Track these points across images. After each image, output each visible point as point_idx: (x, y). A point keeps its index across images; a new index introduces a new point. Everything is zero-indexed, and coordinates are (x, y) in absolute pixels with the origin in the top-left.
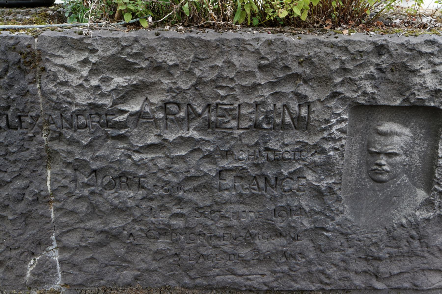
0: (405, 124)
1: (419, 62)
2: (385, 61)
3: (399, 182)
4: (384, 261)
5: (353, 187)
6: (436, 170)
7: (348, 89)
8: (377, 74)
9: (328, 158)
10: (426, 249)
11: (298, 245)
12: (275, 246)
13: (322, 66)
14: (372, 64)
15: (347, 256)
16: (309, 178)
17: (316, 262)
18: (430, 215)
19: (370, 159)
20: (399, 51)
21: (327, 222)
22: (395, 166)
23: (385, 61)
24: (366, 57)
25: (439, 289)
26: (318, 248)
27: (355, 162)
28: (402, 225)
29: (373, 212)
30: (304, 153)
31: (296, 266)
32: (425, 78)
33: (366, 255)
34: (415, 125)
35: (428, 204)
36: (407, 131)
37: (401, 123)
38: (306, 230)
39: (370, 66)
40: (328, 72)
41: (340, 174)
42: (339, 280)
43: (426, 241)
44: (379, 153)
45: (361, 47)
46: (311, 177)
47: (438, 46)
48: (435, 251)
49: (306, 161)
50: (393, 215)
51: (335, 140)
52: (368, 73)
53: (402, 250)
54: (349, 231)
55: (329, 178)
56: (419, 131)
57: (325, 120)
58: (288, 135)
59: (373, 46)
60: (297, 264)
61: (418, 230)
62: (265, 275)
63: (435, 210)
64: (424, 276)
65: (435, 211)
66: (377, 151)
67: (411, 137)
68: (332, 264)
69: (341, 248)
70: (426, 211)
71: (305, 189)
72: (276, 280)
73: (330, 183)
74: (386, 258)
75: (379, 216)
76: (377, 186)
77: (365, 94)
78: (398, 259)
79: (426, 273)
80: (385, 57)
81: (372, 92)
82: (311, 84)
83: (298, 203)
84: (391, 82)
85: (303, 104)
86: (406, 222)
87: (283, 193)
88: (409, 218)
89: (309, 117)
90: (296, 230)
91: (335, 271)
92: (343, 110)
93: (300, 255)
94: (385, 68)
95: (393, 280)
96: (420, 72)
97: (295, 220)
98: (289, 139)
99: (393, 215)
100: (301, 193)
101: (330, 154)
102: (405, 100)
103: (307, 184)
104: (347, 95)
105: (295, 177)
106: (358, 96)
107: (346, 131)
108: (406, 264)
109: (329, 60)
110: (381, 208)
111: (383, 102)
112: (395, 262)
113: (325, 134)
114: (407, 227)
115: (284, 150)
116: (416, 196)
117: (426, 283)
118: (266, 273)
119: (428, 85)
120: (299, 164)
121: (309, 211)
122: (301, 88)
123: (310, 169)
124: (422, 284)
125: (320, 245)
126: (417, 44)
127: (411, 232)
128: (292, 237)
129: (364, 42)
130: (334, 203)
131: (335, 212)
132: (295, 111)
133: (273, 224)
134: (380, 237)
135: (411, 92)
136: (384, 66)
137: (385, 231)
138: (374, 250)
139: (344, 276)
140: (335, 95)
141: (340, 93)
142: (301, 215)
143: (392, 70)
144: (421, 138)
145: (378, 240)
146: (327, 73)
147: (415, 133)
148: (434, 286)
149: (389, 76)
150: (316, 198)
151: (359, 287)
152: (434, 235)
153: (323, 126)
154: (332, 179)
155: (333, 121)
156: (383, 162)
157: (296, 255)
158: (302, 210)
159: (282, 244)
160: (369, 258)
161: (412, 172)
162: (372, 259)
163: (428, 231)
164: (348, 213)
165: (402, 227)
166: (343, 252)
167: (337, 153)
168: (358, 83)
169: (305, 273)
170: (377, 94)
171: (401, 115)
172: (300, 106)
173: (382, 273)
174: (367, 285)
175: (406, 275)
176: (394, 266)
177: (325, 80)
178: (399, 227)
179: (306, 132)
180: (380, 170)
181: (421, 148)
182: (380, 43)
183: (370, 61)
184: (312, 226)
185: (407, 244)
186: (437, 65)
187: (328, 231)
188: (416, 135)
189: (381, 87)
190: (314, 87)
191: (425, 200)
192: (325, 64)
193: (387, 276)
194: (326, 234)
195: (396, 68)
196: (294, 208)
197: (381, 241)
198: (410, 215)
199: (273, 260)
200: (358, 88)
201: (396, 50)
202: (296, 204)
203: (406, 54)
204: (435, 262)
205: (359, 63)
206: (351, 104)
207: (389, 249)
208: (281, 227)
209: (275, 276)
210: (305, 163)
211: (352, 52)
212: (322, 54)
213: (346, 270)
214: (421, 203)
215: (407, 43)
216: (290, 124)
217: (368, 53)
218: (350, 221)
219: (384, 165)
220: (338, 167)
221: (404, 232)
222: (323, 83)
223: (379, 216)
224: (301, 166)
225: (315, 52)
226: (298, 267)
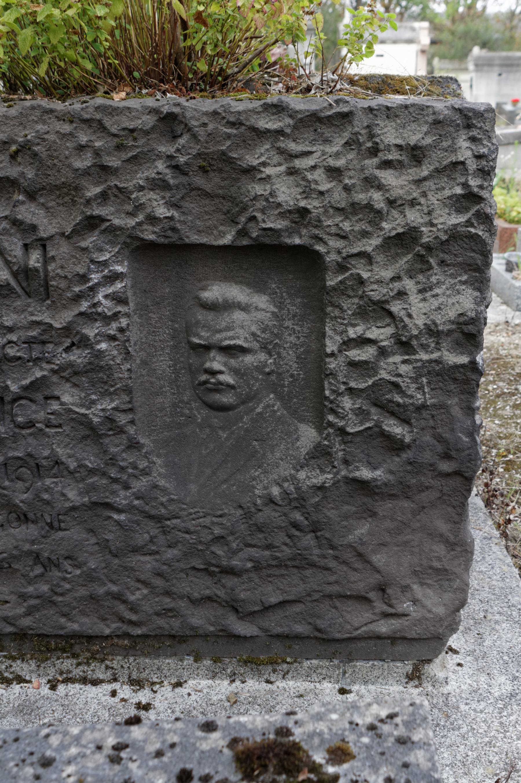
0: (259, 287)
1: (257, 151)
2: (183, 149)
3: (259, 410)
4: (245, 577)
5: (168, 420)
6: (326, 383)
7: (118, 211)
8: (173, 177)
9: (97, 356)
10: (331, 552)
11: (62, 539)
12: (17, 541)
13: (55, 161)
14: (159, 156)
15: (164, 564)
16: (66, 398)
17: (102, 577)
18: (326, 478)
19: (194, 361)
20: (211, 127)
21: (114, 493)
22: (244, 374)
23: (183, 149)
24: (144, 140)
25: (370, 638)
26: (104, 546)
27: (165, 366)
28: (271, 501)
29: (214, 473)
30: (50, 347)
31: (62, 583)
32: (273, 184)
33: (205, 564)
34: (279, 288)
35: (320, 454)
36: (261, 301)
37: (248, 285)
38: (74, 509)
39: (155, 160)
40: (69, 175)
41: (128, 390)
42: (158, 614)
43: (327, 535)
44: (207, 348)
45: (131, 120)
46: (69, 396)
47: (291, 116)
48: (348, 555)
49: (54, 363)
50: (254, 479)
51: (107, 319)
52: (153, 175)
53: (278, 554)
54: (163, 511)
55: (108, 399)
56: (288, 301)
57: (78, 275)
58: (12, 308)
59: (156, 118)
60: (64, 579)
61: (304, 510)
62: (7, 602)
63: (334, 467)
64: (334, 610)
65: (335, 470)
66: (202, 342)
67: (273, 313)
68: (138, 581)
69: (153, 548)
70: (318, 471)
71: (61, 422)
72: (29, 613)
73: (108, 410)
74: (247, 571)
75: (225, 481)
76: (215, 417)
77: (152, 219)
78: (276, 573)
79: (338, 604)
80: (182, 141)
81: (167, 215)
82: (42, 201)
83: (49, 452)
84: (207, 195)
85: (31, 244)
86: (280, 493)
87: (17, 430)
88: (286, 485)
89: (46, 271)
90: (53, 507)
91: (145, 597)
92: (113, 254)
93: (70, 562)
94: (186, 163)
95: (273, 618)
96: (262, 172)
97: (49, 487)
98: (15, 316)
99: (254, 479)
100: (53, 430)
101: (98, 347)
102: (243, 233)
103: (63, 412)
104: (117, 222)
105: (39, 397)
106: (139, 224)
107: (127, 298)
108: (294, 585)
109: (68, 148)
110: (229, 465)
111: (196, 237)
112: (269, 579)
113: (84, 306)
114: (280, 503)
115: (5, 340)
116: (297, 439)
117: (340, 625)
118: (7, 598)
119: (281, 198)
120: (42, 369)
121: (75, 469)
122: (22, 208)
123: (68, 380)
124: (330, 626)
125: (108, 541)
126: (245, 112)
127: (292, 516)
128: (47, 524)
129: (138, 111)
130: (124, 451)
131: (130, 471)
132: (15, 257)
133: (6, 496)
134: (229, 524)
135: (247, 214)
136: (182, 159)
137: (240, 512)
138: (220, 552)
139: (165, 607)
140: (92, 223)
141: (102, 220)
142: (63, 477)
143: (202, 168)
144: (294, 316)
145: (226, 532)
146: (65, 176)
147: (280, 306)
148: (359, 632)
149: (199, 181)
150: (88, 442)
151: (201, 632)
152: (345, 523)
153: (77, 289)
154: (112, 401)
155: (95, 278)
156: (216, 366)
157: (61, 561)
158: (62, 467)
159: (29, 537)
160: (213, 569)
161: (286, 389)
162: (221, 572)
163: (328, 514)
164: (160, 474)
165: (272, 505)
166: (157, 557)
167: (113, 345)
168: (133, 196)
169: (83, 599)
170: (179, 221)
171: (245, 267)
172: (26, 246)
173: (243, 601)
174: (218, 628)
175: (298, 608)
176: (270, 588)
177: (68, 192)
178: (266, 505)
179: (49, 302)
180: (214, 384)
181: (298, 338)
182: (165, 110)
183: (153, 150)
184: (86, 499)
185: (288, 541)
186: (296, 157)
187: (119, 511)
188: (283, 309)
189: (186, 204)
190: (51, 208)
191: (314, 447)
192: (62, 157)
193: (256, 609)
194: (116, 517)
195: (210, 165)
196: (44, 463)
197: (232, 533)
198: (286, 480)
199: (17, 570)
200: (136, 207)
201: (205, 125)
202: (46, 453)
203: (226, 133)
204: (353, 579)
205: (130, 154)
206: (128, 240)
207: (252, 551)
208: (22, 501)
209: (25, 604)
210: (53, 366)
211: (114, 130)
212: (52, 137)
213: (167, 593)
214: (307, 454)
215: (225, 111)
216: (8, 284)
217: (147, 133)
218: (164, 490)
219: (221, 372)
220: (121, 375)
221: (277, 515)
222: (66, 199)
223: (225, 481)
224: (45, 373)
225: (38, 131)
226: (68, 586)
